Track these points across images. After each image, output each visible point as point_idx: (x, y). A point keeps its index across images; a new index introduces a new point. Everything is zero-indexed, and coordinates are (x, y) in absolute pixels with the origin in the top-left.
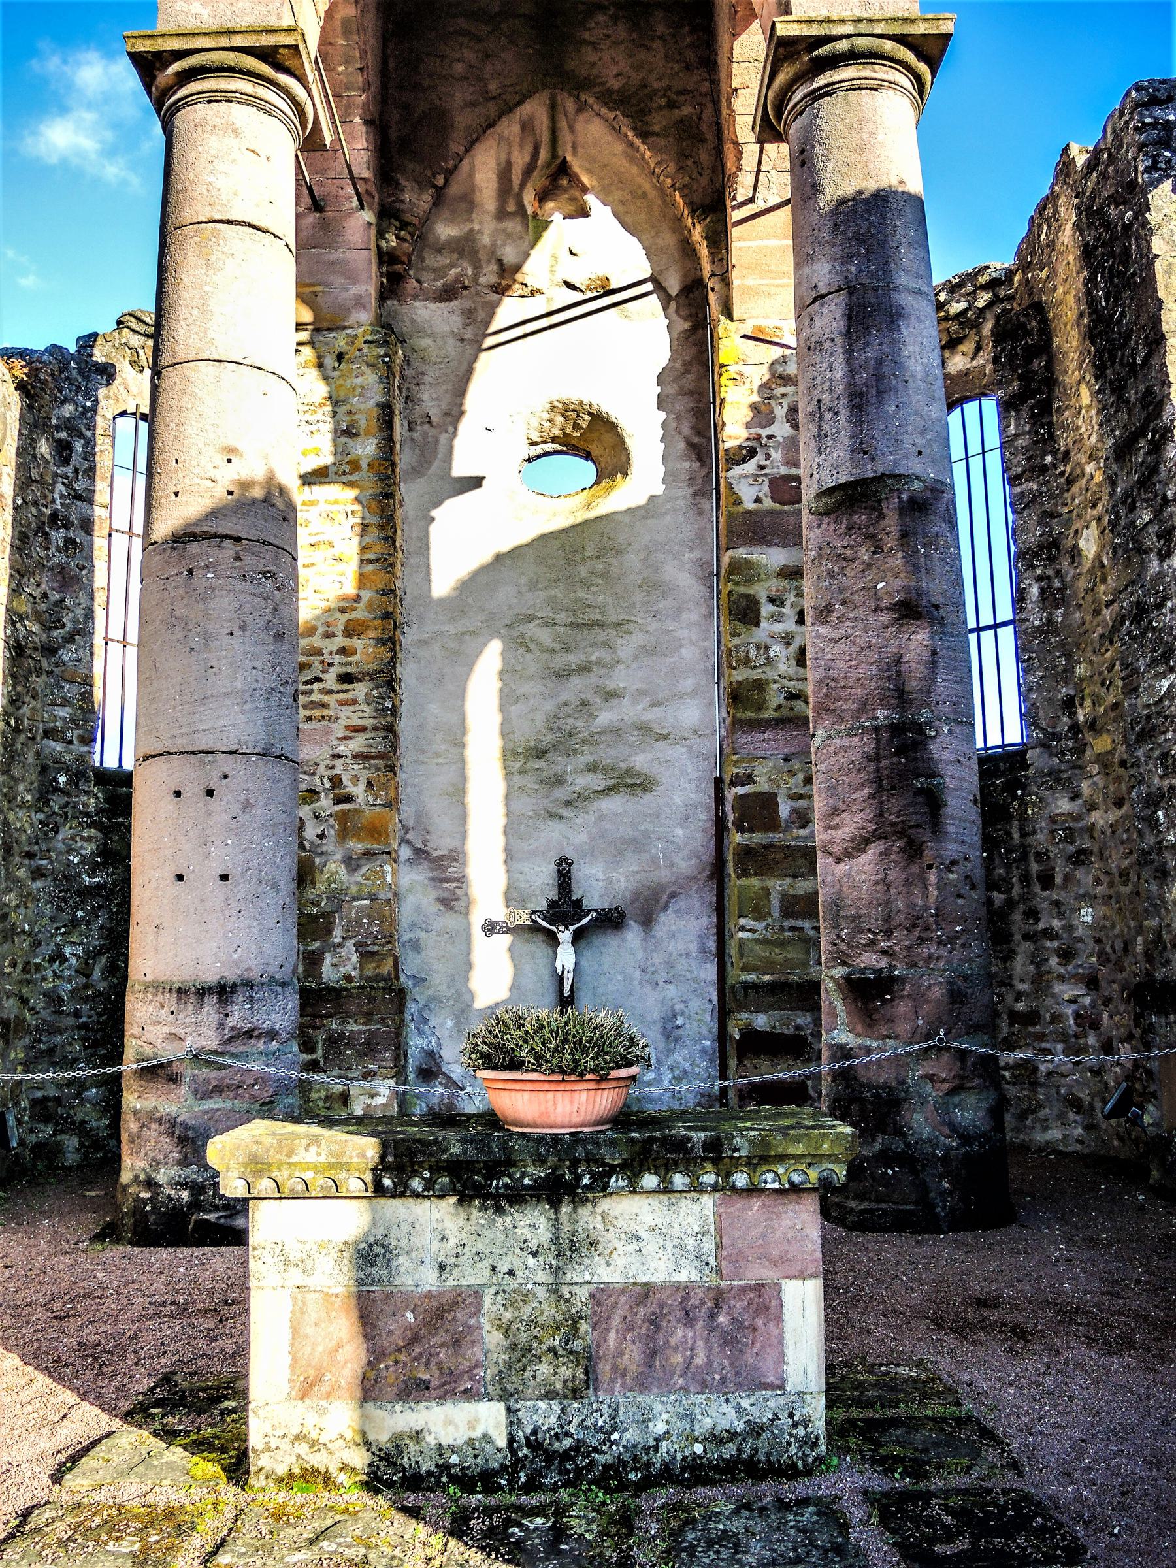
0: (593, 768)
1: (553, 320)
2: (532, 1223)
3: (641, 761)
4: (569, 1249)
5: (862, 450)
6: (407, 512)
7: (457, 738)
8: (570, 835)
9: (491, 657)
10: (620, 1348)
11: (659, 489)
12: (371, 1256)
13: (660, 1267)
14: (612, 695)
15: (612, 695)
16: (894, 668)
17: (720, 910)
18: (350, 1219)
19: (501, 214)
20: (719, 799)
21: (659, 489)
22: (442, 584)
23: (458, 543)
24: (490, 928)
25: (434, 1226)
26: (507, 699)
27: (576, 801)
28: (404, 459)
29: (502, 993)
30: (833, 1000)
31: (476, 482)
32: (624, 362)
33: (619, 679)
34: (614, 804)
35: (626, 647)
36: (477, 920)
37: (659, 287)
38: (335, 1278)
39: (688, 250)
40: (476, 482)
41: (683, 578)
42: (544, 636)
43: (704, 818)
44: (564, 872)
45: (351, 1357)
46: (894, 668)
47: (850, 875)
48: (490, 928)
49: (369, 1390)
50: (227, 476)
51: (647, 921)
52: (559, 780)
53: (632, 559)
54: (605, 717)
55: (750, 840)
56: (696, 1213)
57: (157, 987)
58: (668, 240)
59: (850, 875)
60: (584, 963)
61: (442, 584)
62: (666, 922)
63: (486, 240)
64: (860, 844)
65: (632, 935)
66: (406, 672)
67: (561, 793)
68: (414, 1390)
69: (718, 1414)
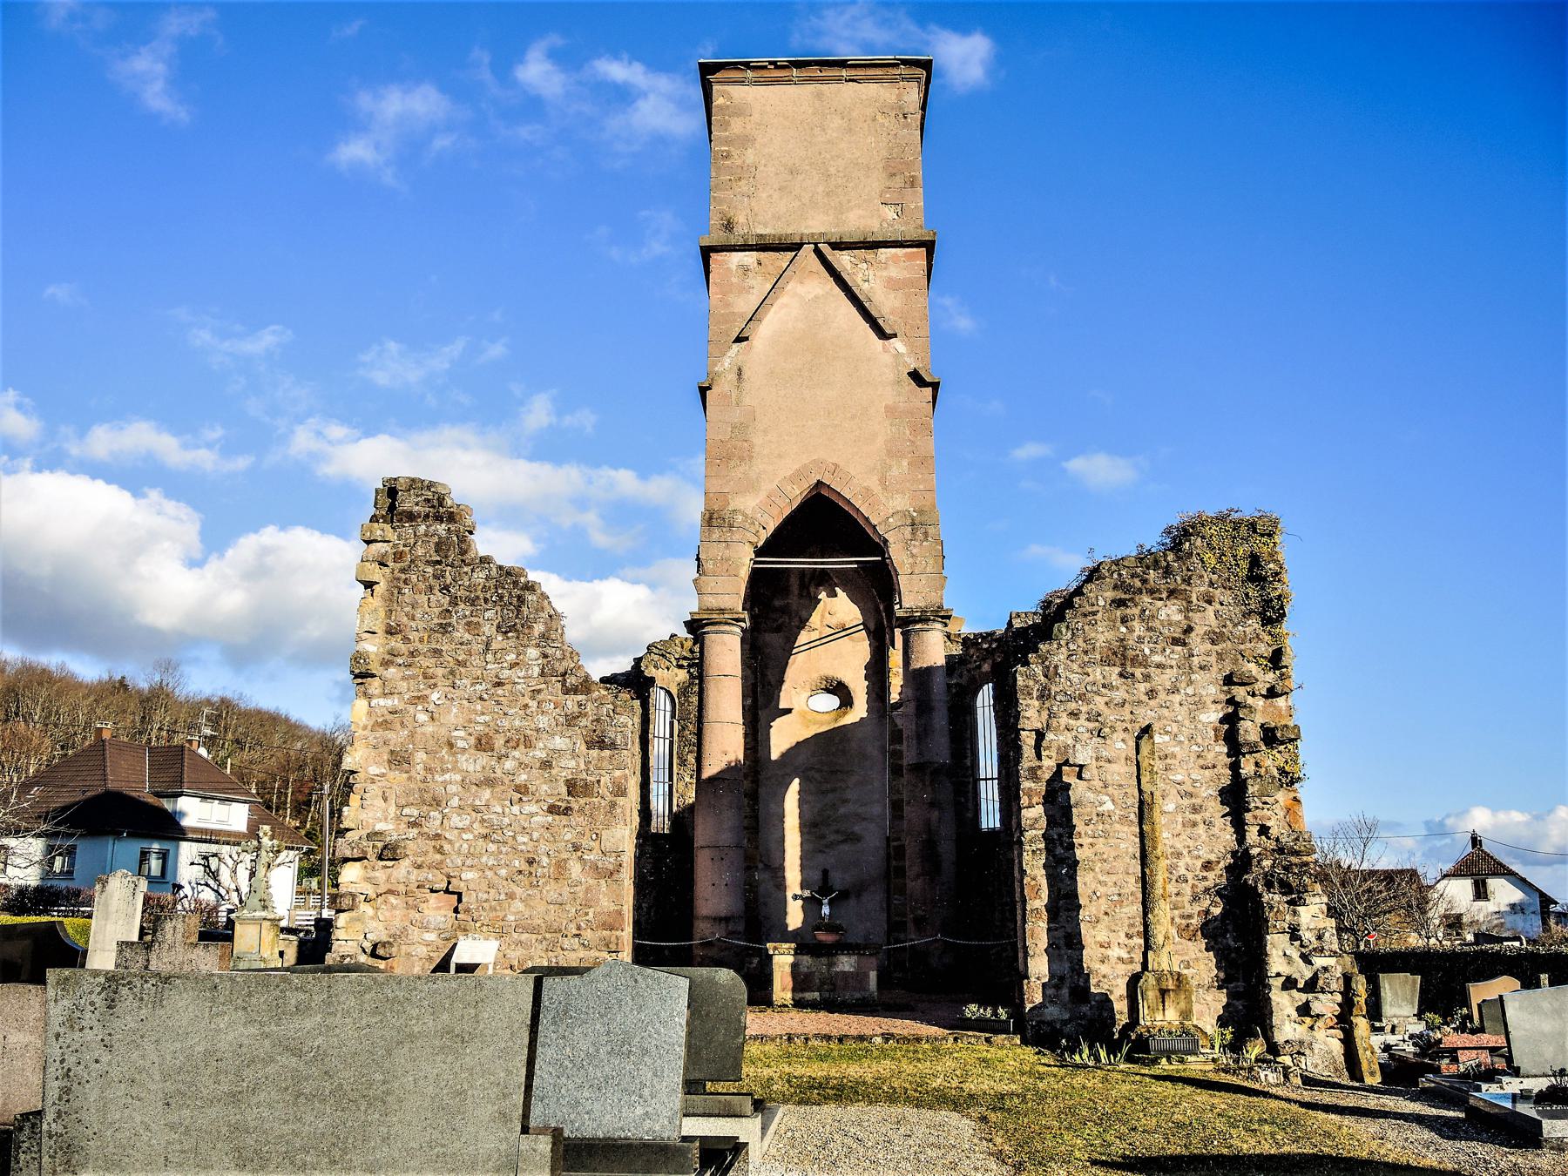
0: (837, 832)
1: (823, 641)
2: (824, 960)
3: (857, 829)
4: (831, 965)
5: (920, 754)
6: (762, 722)
7: (781, 817)
8: (829, 860)
9: (795, 785)
10: (840, 983)
11: (865, 715)
12: (794, 966)
13: (847, 968)
14: (845, 801)
15: (845, 801)
16: (928, 822)
17: (888, 891)
18: (790, 959)
19: (801, 596)
20: (888, 845)
21: (865, 715)
22: (775, 755)
23: (782, 737)
24: (795, 897)
25: (806, 960)
26: (802, 803)
27: (831, 845)
28: (761, 700)
29: (799, 925)
30: (910, 926)
31: (789, 711)
32: (849, 660)
33: (849, 795)
34: (845, 847)
35: (853, 779)
36: (789, 895)
37: (866, 628)
38: (788, 969)
39: (877, 610)
40: (789, 711)
41: (873, 750)
42: (817, 776)
43: (882, 853)
44: (825, 873)
45: (791, 985)
46: (928, 822)
47: (915, 885)
48: (795, 897)
49: (794, 990)
50: (726, 759)
51: (858, 896)
52: (823, 837)
53: (853, 745)
54: (842, 810)
55: (892, 871)
56: (854, 959)
57: (707, 917)
58: (870, 605)
59: (915, 885)
60: (1228, 836)
61: (775, 755)
62: (865, 897)
63: (794, 607)
64: (918, 876)
65: (852, 902)
66: (762, 791)
67: (823, 842)
68: (803, 990)
69: (857, 995)
